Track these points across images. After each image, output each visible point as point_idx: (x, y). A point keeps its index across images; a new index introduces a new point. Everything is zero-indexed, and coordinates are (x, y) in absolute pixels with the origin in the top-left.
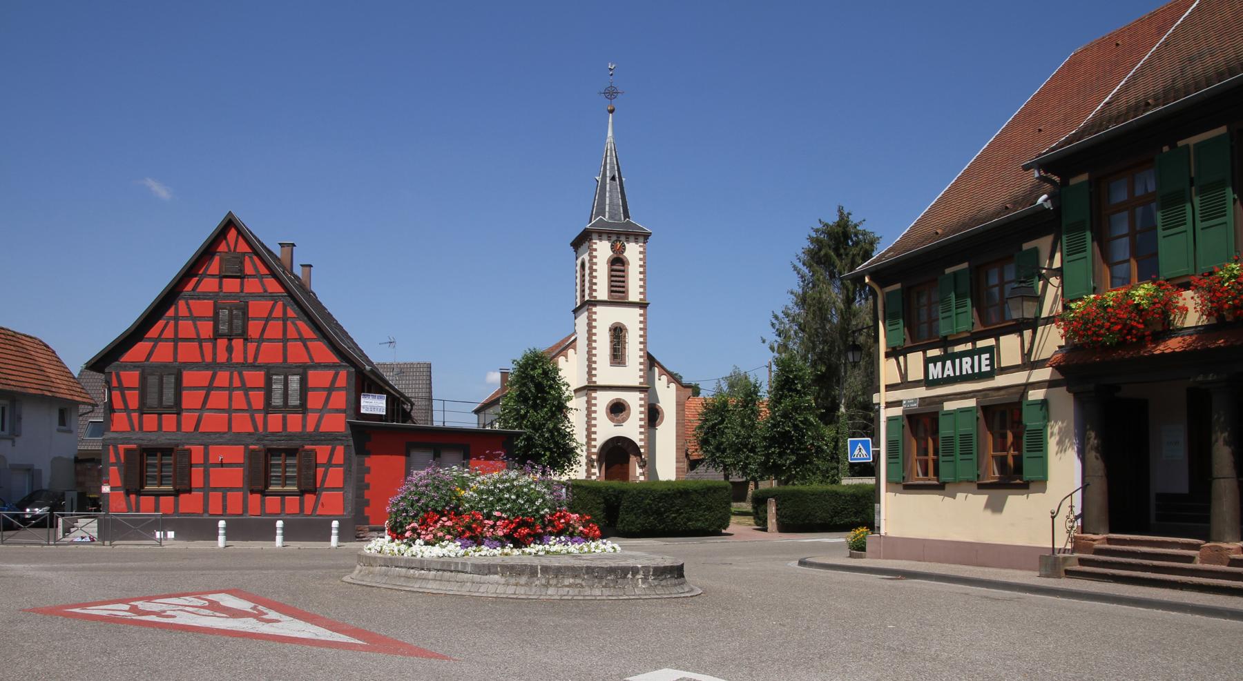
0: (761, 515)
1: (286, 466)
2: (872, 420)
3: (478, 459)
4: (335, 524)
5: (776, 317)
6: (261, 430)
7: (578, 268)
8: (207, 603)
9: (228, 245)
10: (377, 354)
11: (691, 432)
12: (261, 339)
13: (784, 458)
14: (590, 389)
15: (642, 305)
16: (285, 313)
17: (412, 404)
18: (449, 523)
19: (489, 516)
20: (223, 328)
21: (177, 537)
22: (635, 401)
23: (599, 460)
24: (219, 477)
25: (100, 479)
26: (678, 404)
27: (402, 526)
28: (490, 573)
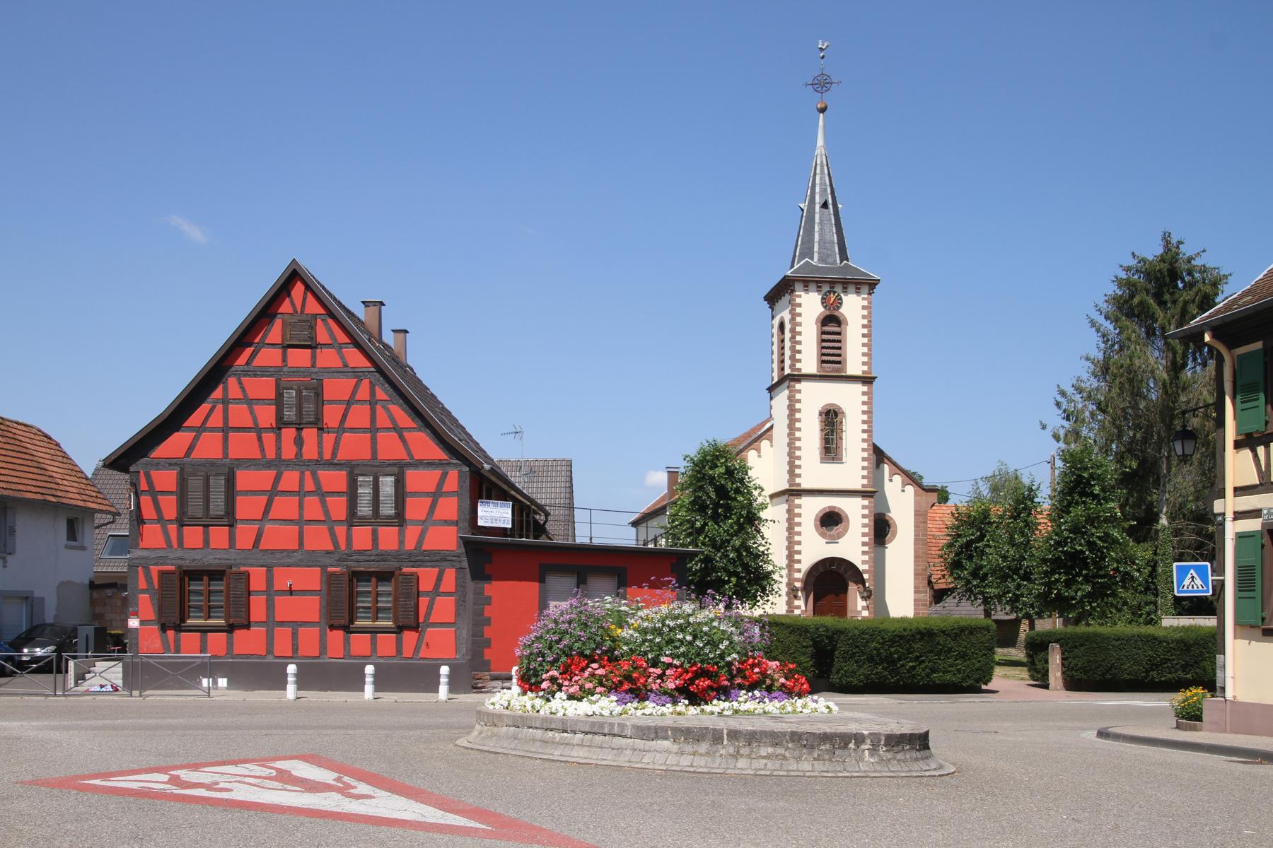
0: (1039, 666)
1: (378, 594)
2: (1211, 537)
3: (640, 587)
4: (444, 670)
5: (1063, 394)
6: (343, 546)
7: (775, 330)
8: (274, 773)
9: (293, 304)
10: (498, 447)
11: (935, 552)
12: (342, 429)
13: (1076, 584)
14: (793, 493)
15: (867, 380)
16: (373, 393)
17: (547, 514)
18: (601, 672)
19: (655, 663)
20: (290, 414)
21: (231, 685)
22: (855, 510)
23: (805, 589)
24: (286, 608)
25: (125, 609)
27: (536, 675)
28: (657, 737)
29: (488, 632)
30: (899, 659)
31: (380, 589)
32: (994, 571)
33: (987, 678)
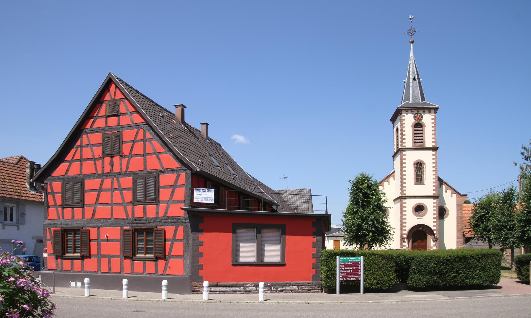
6: (130, 216)
7: (395, 133)
9: (111, 96)
14: (403, 197)
15: (435, 149)
16: (145, 136)
22: (430, 205)
23: (408, 238)
26: (458, 205)
29: (201, 261)
30: (447, 272)
31: (149, 238)
32: (494, 227)
33: (497, 278)
